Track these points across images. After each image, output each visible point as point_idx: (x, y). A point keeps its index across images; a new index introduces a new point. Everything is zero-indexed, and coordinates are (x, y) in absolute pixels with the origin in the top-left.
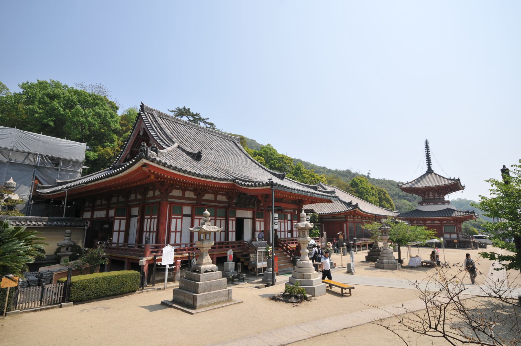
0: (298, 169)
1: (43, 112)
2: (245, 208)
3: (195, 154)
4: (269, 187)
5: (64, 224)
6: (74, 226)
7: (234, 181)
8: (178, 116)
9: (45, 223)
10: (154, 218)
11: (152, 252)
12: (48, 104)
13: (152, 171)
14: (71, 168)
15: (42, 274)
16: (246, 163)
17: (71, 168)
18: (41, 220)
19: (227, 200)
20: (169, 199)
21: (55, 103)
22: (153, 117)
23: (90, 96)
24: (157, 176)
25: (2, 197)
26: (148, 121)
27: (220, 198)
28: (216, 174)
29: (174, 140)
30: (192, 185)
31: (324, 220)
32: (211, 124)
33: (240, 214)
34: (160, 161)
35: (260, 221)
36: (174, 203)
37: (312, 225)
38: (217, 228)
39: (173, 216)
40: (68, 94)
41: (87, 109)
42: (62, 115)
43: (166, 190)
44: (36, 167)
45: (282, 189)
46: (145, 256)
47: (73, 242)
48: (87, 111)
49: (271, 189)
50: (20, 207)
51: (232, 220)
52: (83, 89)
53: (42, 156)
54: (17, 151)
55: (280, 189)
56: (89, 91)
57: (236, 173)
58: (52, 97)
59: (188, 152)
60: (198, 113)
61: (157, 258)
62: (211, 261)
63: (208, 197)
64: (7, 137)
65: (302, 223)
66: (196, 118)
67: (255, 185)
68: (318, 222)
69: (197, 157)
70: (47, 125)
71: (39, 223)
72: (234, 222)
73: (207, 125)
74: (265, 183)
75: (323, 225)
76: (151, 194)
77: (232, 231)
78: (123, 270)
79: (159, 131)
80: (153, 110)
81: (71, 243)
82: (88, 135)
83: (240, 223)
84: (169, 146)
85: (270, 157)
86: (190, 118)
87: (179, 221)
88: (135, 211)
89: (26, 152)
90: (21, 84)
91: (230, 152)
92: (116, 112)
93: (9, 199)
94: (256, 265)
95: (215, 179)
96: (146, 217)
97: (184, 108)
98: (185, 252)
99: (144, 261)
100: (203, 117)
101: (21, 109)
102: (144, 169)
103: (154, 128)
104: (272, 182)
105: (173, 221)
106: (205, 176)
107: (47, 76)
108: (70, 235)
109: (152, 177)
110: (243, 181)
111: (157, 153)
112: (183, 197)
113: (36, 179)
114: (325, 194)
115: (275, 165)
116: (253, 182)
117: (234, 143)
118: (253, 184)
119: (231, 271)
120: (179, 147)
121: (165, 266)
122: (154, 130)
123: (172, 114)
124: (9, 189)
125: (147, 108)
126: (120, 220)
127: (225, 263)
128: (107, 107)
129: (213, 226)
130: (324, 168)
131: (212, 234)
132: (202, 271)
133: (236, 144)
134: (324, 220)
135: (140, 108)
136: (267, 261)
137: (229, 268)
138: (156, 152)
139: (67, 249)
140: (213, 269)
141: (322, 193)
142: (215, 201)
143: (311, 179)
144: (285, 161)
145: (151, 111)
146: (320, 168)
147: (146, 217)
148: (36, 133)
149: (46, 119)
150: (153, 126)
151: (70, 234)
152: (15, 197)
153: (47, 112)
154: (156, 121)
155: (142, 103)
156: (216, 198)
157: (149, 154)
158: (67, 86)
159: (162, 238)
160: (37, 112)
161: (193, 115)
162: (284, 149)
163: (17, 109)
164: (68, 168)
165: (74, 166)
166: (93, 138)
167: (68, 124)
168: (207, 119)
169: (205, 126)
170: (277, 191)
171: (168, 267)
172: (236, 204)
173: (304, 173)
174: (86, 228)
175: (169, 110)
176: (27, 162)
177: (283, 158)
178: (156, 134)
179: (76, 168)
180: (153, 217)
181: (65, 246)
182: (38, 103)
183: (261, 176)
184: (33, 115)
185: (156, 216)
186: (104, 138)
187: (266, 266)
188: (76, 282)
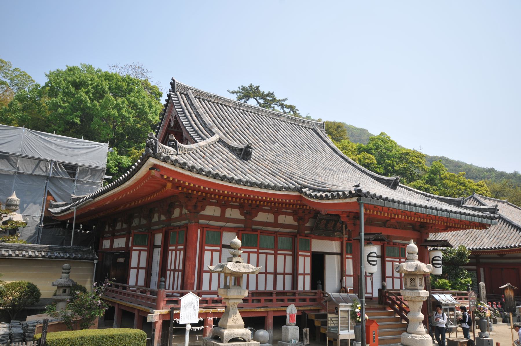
0: (435, 172)
1: (68, 106)
2: (328, 236)
3: (242, 149)
4: (355, 199)
5: (68, 255)
6: (80, 259)
7: (300, 190)
8: (242, 99)
9: (43, 254)
10: (180, 250)
11: (169, 302)
12: (74, 94)
13: (165, 177)
14: (90, 178)
15: (28, 326)
16: (331, 163)
17: (90, 178)
18: (39, 250)
19: (296, 223)
20: (201, 221)
21: (82, 94)
22: (189, 99)
23: (123, 80)
24: (176, 185)
25: (1, 220)
26: (180, 105)
27: (283, 219)
28: (269, 180)
29: (215, 129)
30: (215, 195)
31: (481, 260)
32: (291, 107)
33: (318, 245)
34: (176, 161)
35: (285, 255)
36: (208, 226)
37: (429, 268)
38: (252, 268)
39: (206, 248)
40: (96, 79)
41: (120, 98)
42: (88, 108)
43: (195, 206)
44: (48, 178)
45: (380, 203)
46: (157, 308)
47: (72, 281)
48: (120, 100)
49: (359, 204)
50: (30, 230)
51: (304, 256)
52: (114, 72)
53: (55, 163)
54: (25, 157)
55: (374, 202)
56: (124, 74)
57: (306, 177)
58: (78, 85)
59: (232, 147)
60: (271, 92)
61: (176, 312)
62: (242, 323)
63: (262, 217)
64: (20, 140)
65: (409, 263)
66: (269, 100)
67: (333, 197)
68: (469, 264)
69: (245, 154)
70: (74, 124)
71: (37, 253)
72: (308, 260)
73: (285, 109)
74: (347, 193)
75: (482, 270)
76: (177, 213)
77: (304, 274)
78: (133, 328)
79: (195, 118)
80: (188, 88)
81: (68, 283)
82: (121, 134)
83: (318, 262)
84: (203, 139)
85: (385, 153)
86: (259, 101)
87: (216, 255)
88: (158, 239)
89: (37, 159)
90: (48, 73)
91: (306, 147)
92: (159, 100)
93: (10, 220)
94: (336, 334)
95: (267, 187)
96: (171, 248)
97: (251, 86)
98: (220, 304)
99: (155, 316)
100: (278, 97)
101: (44, 105)
102: (153, 172)
103: (188, 114)
104: (360, 191)
105: (207, 255)
106: (250, 183)
107: (77, 60)
108: (68, 271)
109: (169, 186)
110: (314, 190)
111: (176, 149)
112: (222, 218)
113: (49, 194)
114: (476, 213)
115: (393, 167)
116: (329, 191)
117: (316, 131)
118: (329, 194)
119: (293, 341)
120: (220, 141)
121: (185, 325)
122: (187, 118)
123: (234, 98)
124: (10, 207)
125: (180, 86)
126: (140, 251)
127: (283, 327)
128: (145, 93)
129: (246, 265)
130: (491, 170)
131: (245, 276)
132: (226, 338)
133: (318, 134)
134: (481, 260)
135: (170, 87)
136: (355, 328)
137: (290, 336)
138: (175, 147)
139: (64, 291)
140: (245, 338)
141: (472, 212)
142: (276, 224)
143: (460, 190)
144: (411, 159)
145: (185, 91)
146: (484, 170)
147: (171, 248)
148: (92, 140)
149: (71, 115)
150: (186, 111)
151: (69, 269)
152: (17, 217)
153: (72, 105)
154: (192, 105)
155: (172, 79)
156: (276, 219)
157: (158, 150)
158: (100, 71)
159: (189, 281)
160: (61, 107)
161: (263, 96)
162: (408, 138)
163: (39, 105)
164: (86, 180)
165: (93, 175)
166: (127, 137)
167: (96, 119)
168: (284, 100)
169: (282, 111)
170: (367, 207)
171: (189, 327)
172: (311, 229)
173: (446, 178)
174: (95, 262)
175: (229, 91)
176: (37, 172)
177: (407, 154)
178: (190, 123)
179: (96, 177)
180: (179, 247)
181: (62, 287)
182: (63, 95)
183: (344, 178)
184: (56, 111)
185: (182, 247)
186: (140, 137)
187: (354, 337)
188: (52, 342)
